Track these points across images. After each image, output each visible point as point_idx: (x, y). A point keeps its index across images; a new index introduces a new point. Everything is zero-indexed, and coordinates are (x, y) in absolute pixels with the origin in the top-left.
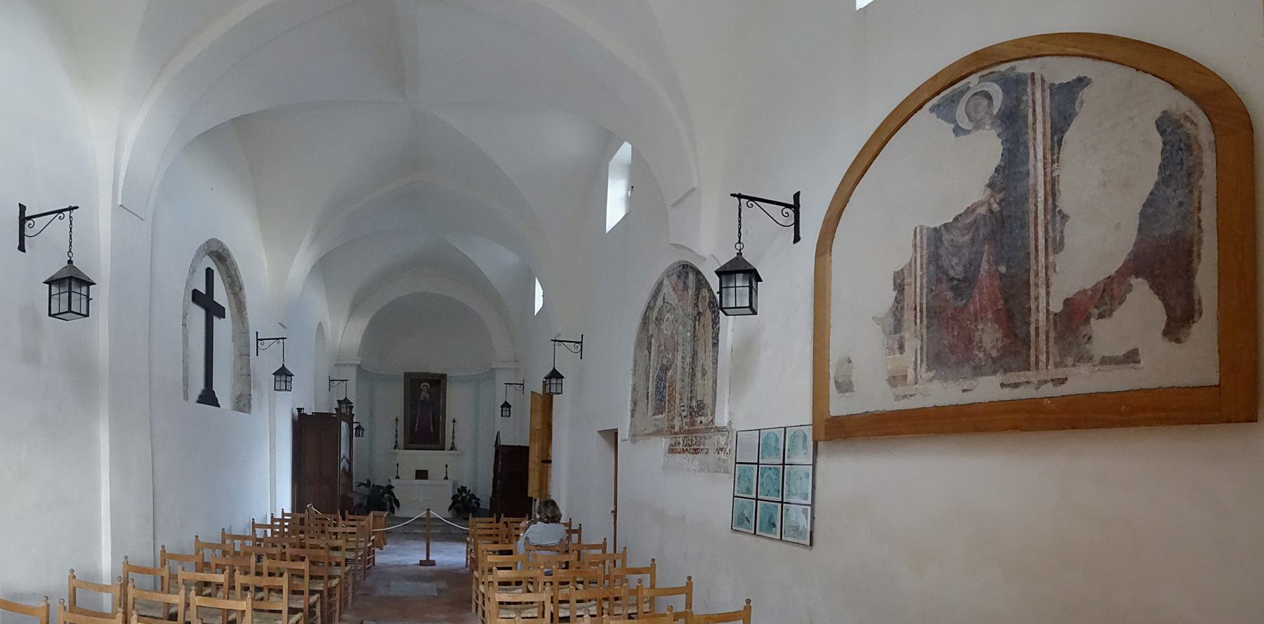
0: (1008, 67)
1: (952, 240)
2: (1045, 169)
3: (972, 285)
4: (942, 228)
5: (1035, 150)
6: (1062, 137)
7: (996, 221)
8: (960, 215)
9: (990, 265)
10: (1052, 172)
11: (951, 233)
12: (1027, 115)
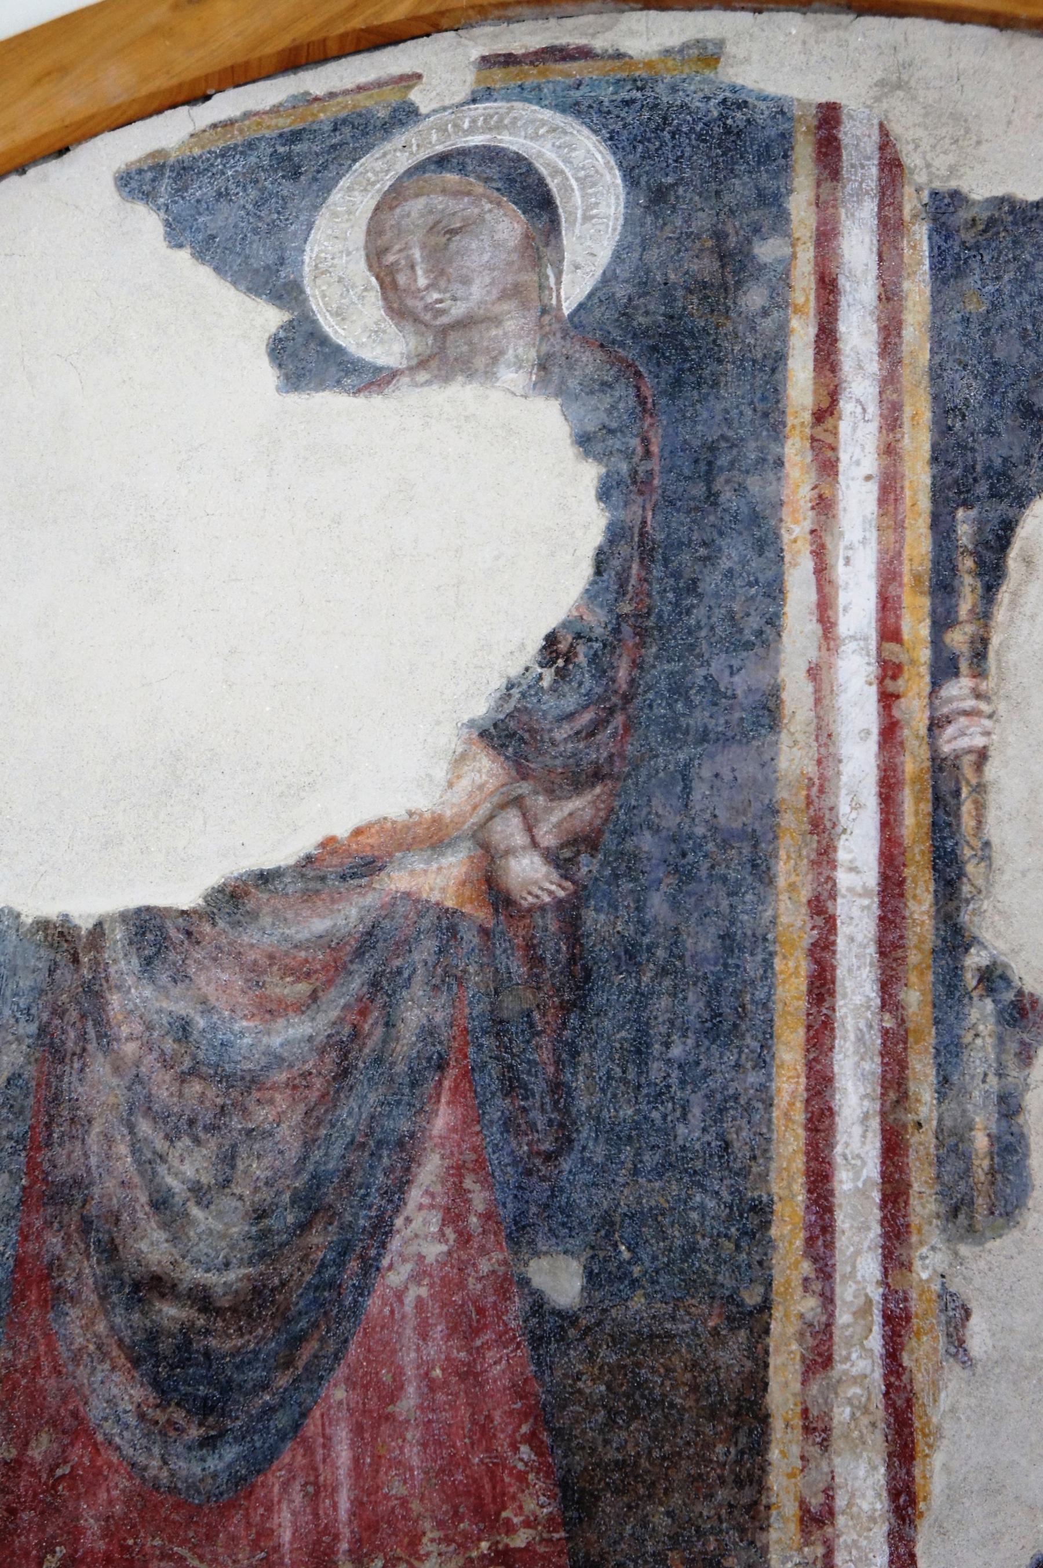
0: (675, 41)
1: (183, 1029)
2: (887, 699)
3: (306, 1353)
4: (118, 934)
5: (822, 570)
6: (1007, 528)
7: (535, 961)
8: (265, 878)
9: (464, 1238)
10: (935, 725)
11: (180, 977)
12: (781, 358)
